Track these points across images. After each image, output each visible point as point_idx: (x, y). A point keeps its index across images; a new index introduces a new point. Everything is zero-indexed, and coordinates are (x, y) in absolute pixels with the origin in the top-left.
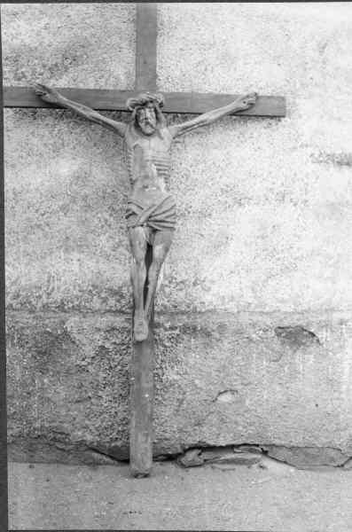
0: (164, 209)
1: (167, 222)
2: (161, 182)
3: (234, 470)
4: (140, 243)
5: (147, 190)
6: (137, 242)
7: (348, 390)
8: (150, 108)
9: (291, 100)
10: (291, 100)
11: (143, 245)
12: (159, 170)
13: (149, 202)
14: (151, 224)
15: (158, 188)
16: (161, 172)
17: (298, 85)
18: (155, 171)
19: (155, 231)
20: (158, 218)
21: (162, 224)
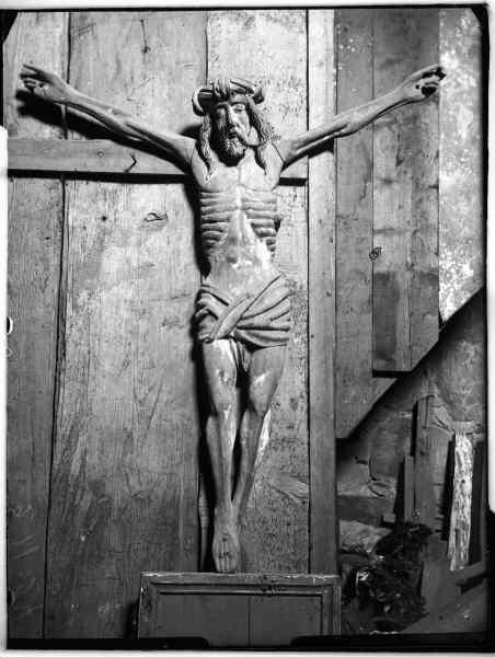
0: (268, 302)
1: (246, 318)
2: (261, 248)
3: (292, 493)
4: (222, 374)
5: (235, 266)
6: (217, 372)
7: (155, 169)
8: (437, 531)
9: (429, 551)
10: (429, 551)
11: (230, 374)
12: (254, 226)
13: (238, 291)
14: (243, 333)
15: (256, 261)
16: (259, 230)
17: (456, 143)
18: (249, 230)
19: (252, 348)
20: (257, 321)
21: (263, 333)
